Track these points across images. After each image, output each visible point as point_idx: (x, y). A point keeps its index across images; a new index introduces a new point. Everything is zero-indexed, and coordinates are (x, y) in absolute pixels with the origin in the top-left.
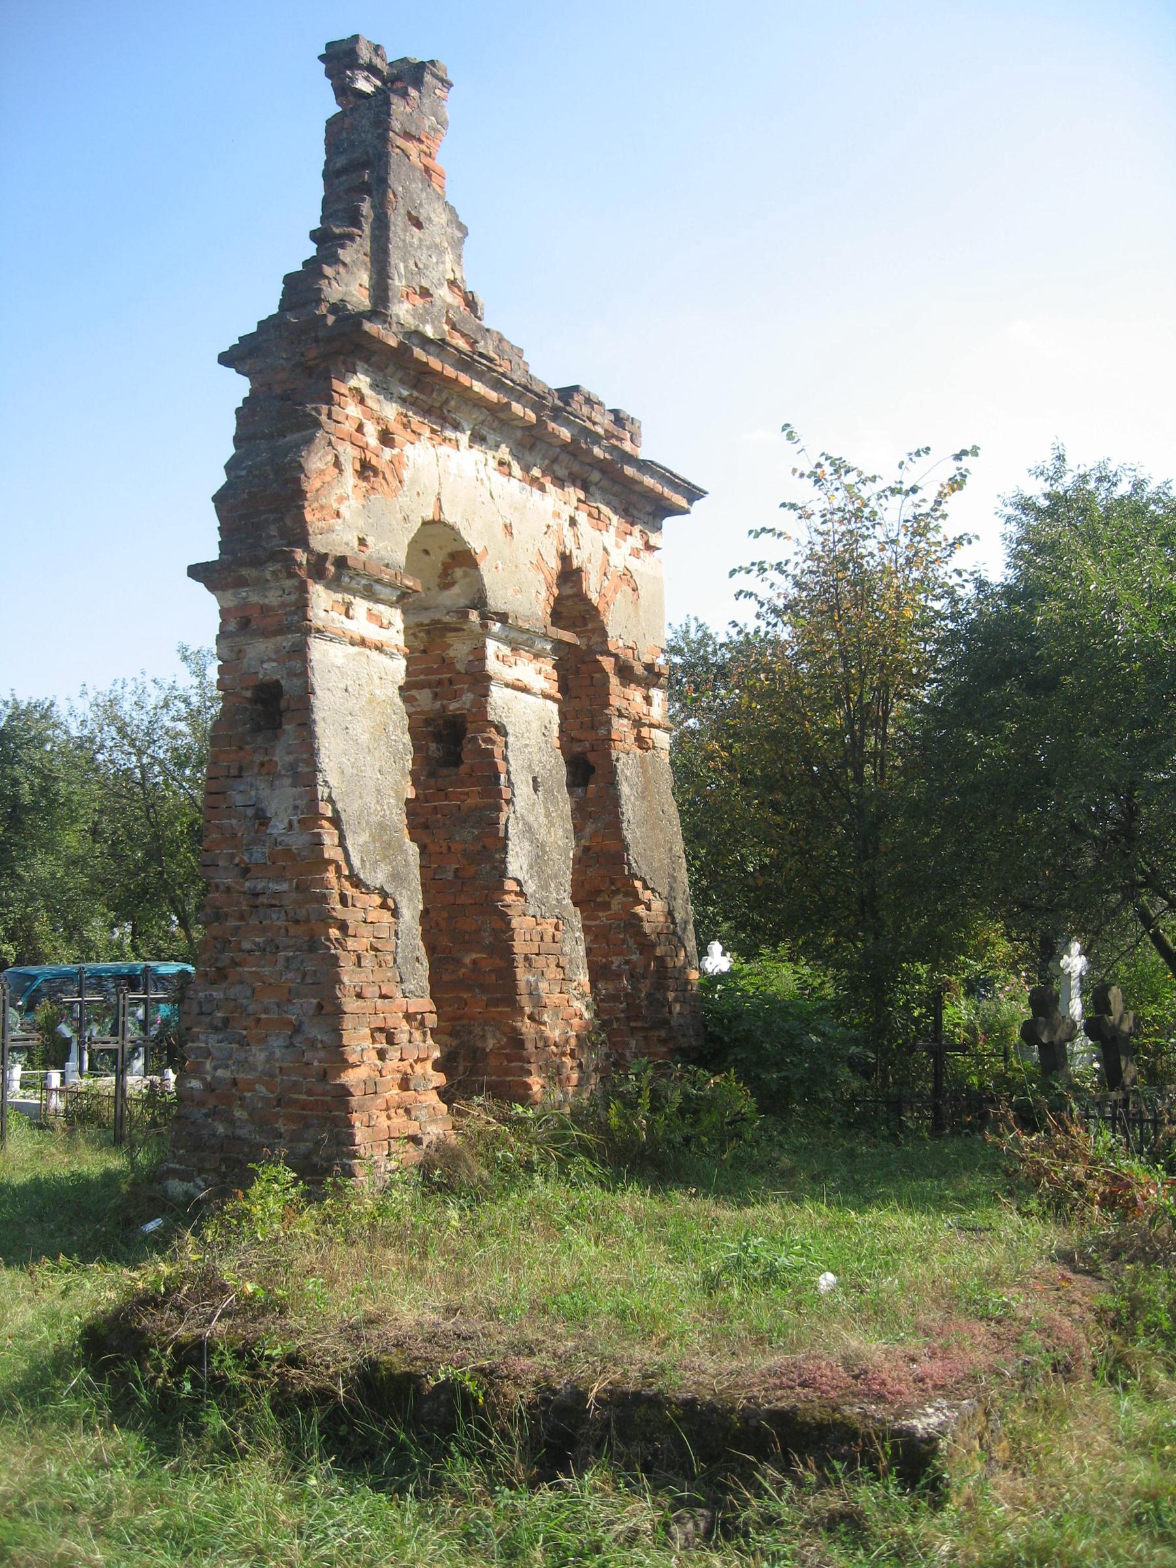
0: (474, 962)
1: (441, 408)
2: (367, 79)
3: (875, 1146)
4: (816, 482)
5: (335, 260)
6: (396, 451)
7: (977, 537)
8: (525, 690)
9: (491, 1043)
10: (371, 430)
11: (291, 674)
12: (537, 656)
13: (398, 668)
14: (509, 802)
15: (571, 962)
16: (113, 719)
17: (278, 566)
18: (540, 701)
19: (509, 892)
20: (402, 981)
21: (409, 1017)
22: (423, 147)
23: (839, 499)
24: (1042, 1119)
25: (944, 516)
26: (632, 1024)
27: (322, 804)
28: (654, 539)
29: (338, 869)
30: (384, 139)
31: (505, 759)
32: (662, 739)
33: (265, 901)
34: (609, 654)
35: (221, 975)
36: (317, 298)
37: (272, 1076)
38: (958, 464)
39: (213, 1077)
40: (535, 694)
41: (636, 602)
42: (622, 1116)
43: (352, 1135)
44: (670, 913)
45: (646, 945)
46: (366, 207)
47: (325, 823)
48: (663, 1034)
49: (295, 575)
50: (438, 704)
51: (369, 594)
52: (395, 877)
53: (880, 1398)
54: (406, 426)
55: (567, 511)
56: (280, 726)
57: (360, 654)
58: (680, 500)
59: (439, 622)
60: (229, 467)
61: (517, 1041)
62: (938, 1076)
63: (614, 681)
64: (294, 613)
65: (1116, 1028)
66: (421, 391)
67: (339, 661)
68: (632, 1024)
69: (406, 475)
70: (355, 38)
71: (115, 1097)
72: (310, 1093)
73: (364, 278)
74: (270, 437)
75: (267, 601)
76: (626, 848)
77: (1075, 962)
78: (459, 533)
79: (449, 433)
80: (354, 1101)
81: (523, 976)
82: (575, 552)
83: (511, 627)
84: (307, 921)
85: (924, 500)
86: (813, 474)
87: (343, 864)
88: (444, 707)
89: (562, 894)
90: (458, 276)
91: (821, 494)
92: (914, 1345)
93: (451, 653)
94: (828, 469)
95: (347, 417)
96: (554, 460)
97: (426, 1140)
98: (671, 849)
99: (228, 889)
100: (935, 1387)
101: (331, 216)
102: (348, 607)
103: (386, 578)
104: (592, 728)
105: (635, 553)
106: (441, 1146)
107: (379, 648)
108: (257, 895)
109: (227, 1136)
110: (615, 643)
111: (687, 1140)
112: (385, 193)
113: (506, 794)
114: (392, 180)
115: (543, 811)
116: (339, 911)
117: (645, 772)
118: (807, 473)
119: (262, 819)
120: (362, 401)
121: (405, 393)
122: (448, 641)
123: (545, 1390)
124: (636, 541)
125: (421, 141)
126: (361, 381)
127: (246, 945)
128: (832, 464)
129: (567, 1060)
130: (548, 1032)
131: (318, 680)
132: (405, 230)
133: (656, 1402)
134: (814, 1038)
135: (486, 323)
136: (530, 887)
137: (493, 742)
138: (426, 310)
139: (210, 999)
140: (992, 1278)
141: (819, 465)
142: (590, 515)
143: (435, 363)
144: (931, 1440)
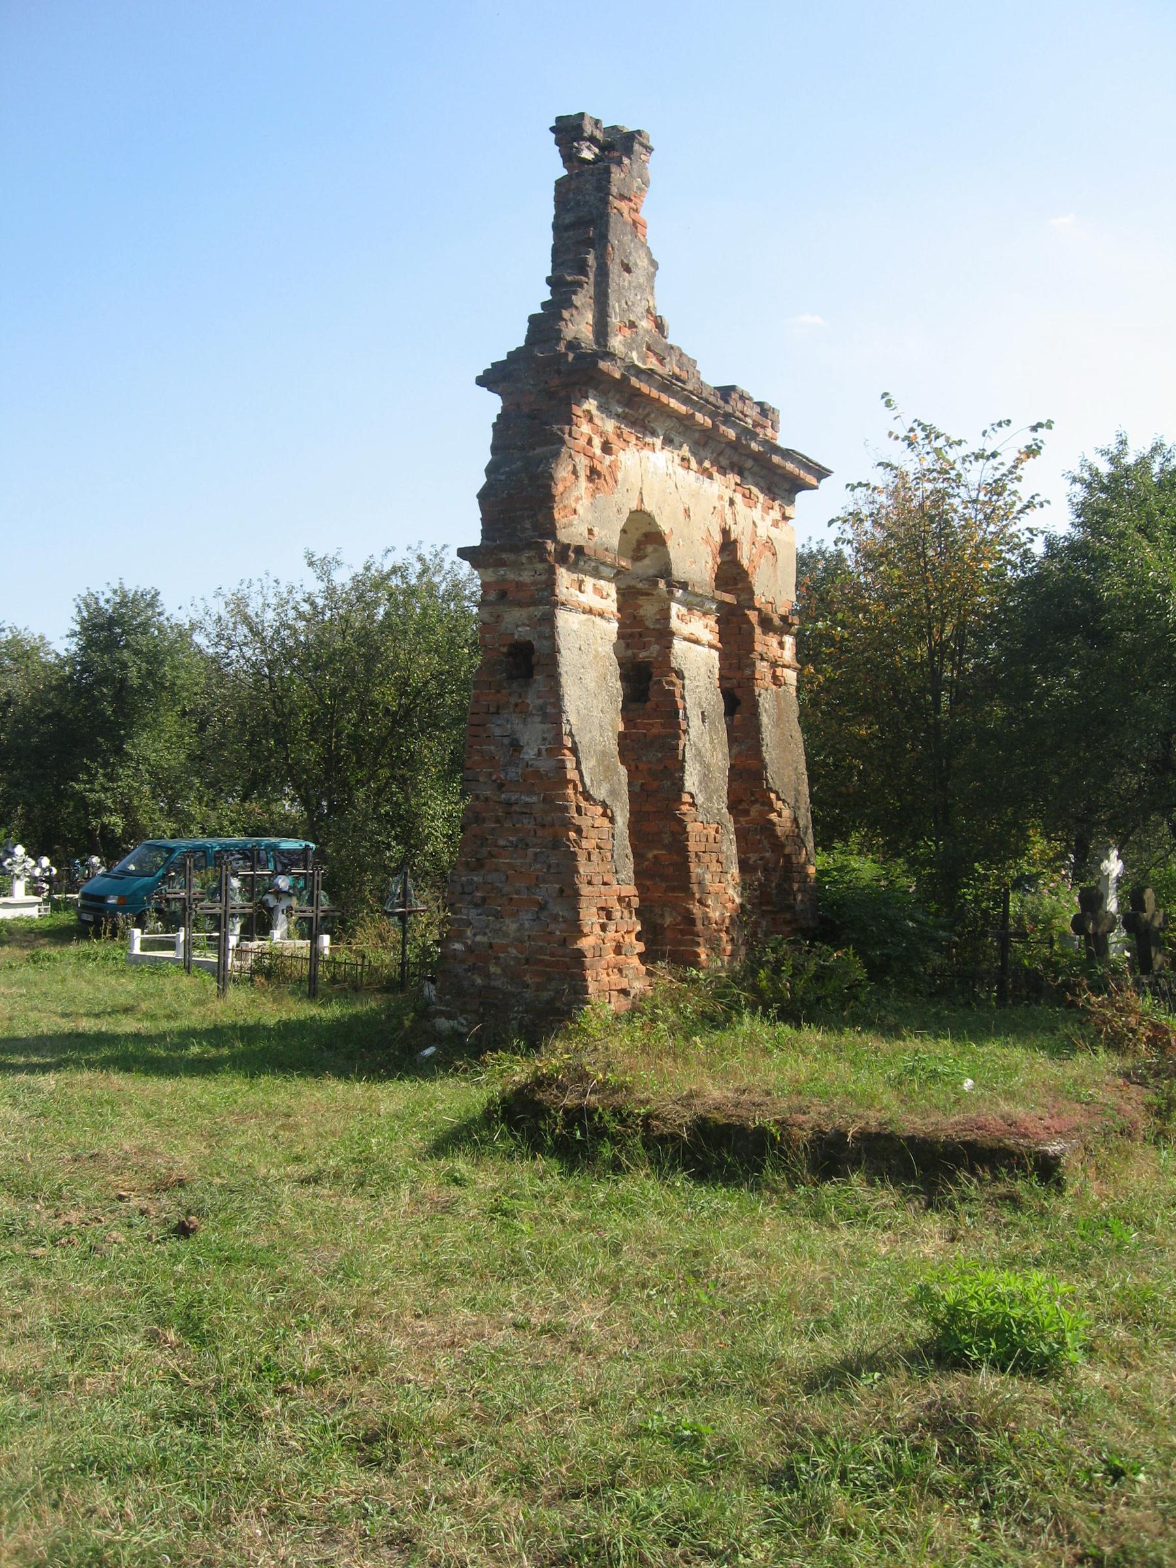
0: (655, 857)
1: (643, 420)
2: (589, 148)
3: (955, 1011)
4: (909, 445)
5: (570, 305)
6: (613, 458)
7: (1048, 502)
8: (696, 642)
9: (668, 921)
10: (597, 442)
11: (541, 636)
12: (705, 614)
13: (612, 628)
14: (685, 732)
15: (727, 858)
16: (246, 620)
17: (532, 553)
18: (706, 650)
19: (685, 803)
20: (617, 872)
21: (620, 899)
22: (632, 205)
23: (929, 461)
24: (1107, 985)
25: (1019, 479)
26: (764, 908)
27: (565, 737)
28: (789, 511)
29: (575, 787)
30: (606, 203)
31: (683, 697)
32: (791, 676)
33: (518, 809)
34: (755, 609)
35: (480, 865)
36: (557, 336)
37: (522, 942)
38: (1035, 435)
39: (473, 941)
40: (703, 645)
41: (774, 565)
42: (770, 979)
43: (586, 987)
44: (795, 820)
45: (777, 845)
46: (591, 259)
47: (566, 752)
48: (788, 916)
49: (545, 561)
50: (630, 653)
51: (596, 574)
52: (613, 792)
53: (1025, 1136)
54: (620, 436)
55: (728, 494)
56: (531, 676)
57: (588, 620)
58: (810, 479)
59: (634, 587)
60: (490, 471)
61: (690, 920)
62: (1003, 958)
63: (758, 630)
64: (545, 590)
65: (1148, 924)
66: (631, 408)
67: (575, 626)
68: (764, 908)
69: (620, 476)
70: (581, 115)
71: (310, 959)
72: (552, 955)
73: (589, 317)
74: (522, 448)
75: (521, 579)
76: (765, 768)
77: (1113, 866)
78: (654, 519)
79: (648, 440)
80: (588, 961)
81: (695, 870)
82: (733, 527)
83: (690, 593)
84: (553, 825)
85: (1002, 464)
86: (907, 438)
87: (578, 783)
88: (635, 656)
89: (721, 805)
90: (651, 304)
91: (912, 456)
92: (1040, 1111)
93: (642, 612)
94: (920, 434)
95: (582, 434)
96: (721, 454)
97: (632, 993)
98: (796, 768)
99: (487, 799)
100: (1056, 1132)
101: (562, 264)
102: (581, 583)
103: (609, 561)
104: (739, 668)
105: (775, 524)
106: (642, 997)
107: (601, 615)
108: (511, 804)
109: (484, 987)
110: (759, 600)
111: (818, 1000)
112: (605, 247)
113: (684, 726)
114: (611, 236)
115: (708, 738)
116: (577, 820)
117: (779, 704)
118: (902, 436)
119: (516, 746)
120: (591, 420)
121: (620, 410)
122: (640, 602)
123: (819, 1132)
124: (775, 514)
125: (630, 200)
126: (591, 405)
127: (502, 842)
128: (924, 429)
129: (723, 935)
130: (711, 914)
131: (563, 642)
132: (619, 276)
133: (891, 1137)
134: (910, 924)
135: (670, 341)
136: (700, 800)
137: (674, 684)
138: (632, 339)
139: (471, 882)
140: (1079, 1081)
141: (912, 430)
142: (744, 495)
143: (645, 388)
144: (1056, 1158)
